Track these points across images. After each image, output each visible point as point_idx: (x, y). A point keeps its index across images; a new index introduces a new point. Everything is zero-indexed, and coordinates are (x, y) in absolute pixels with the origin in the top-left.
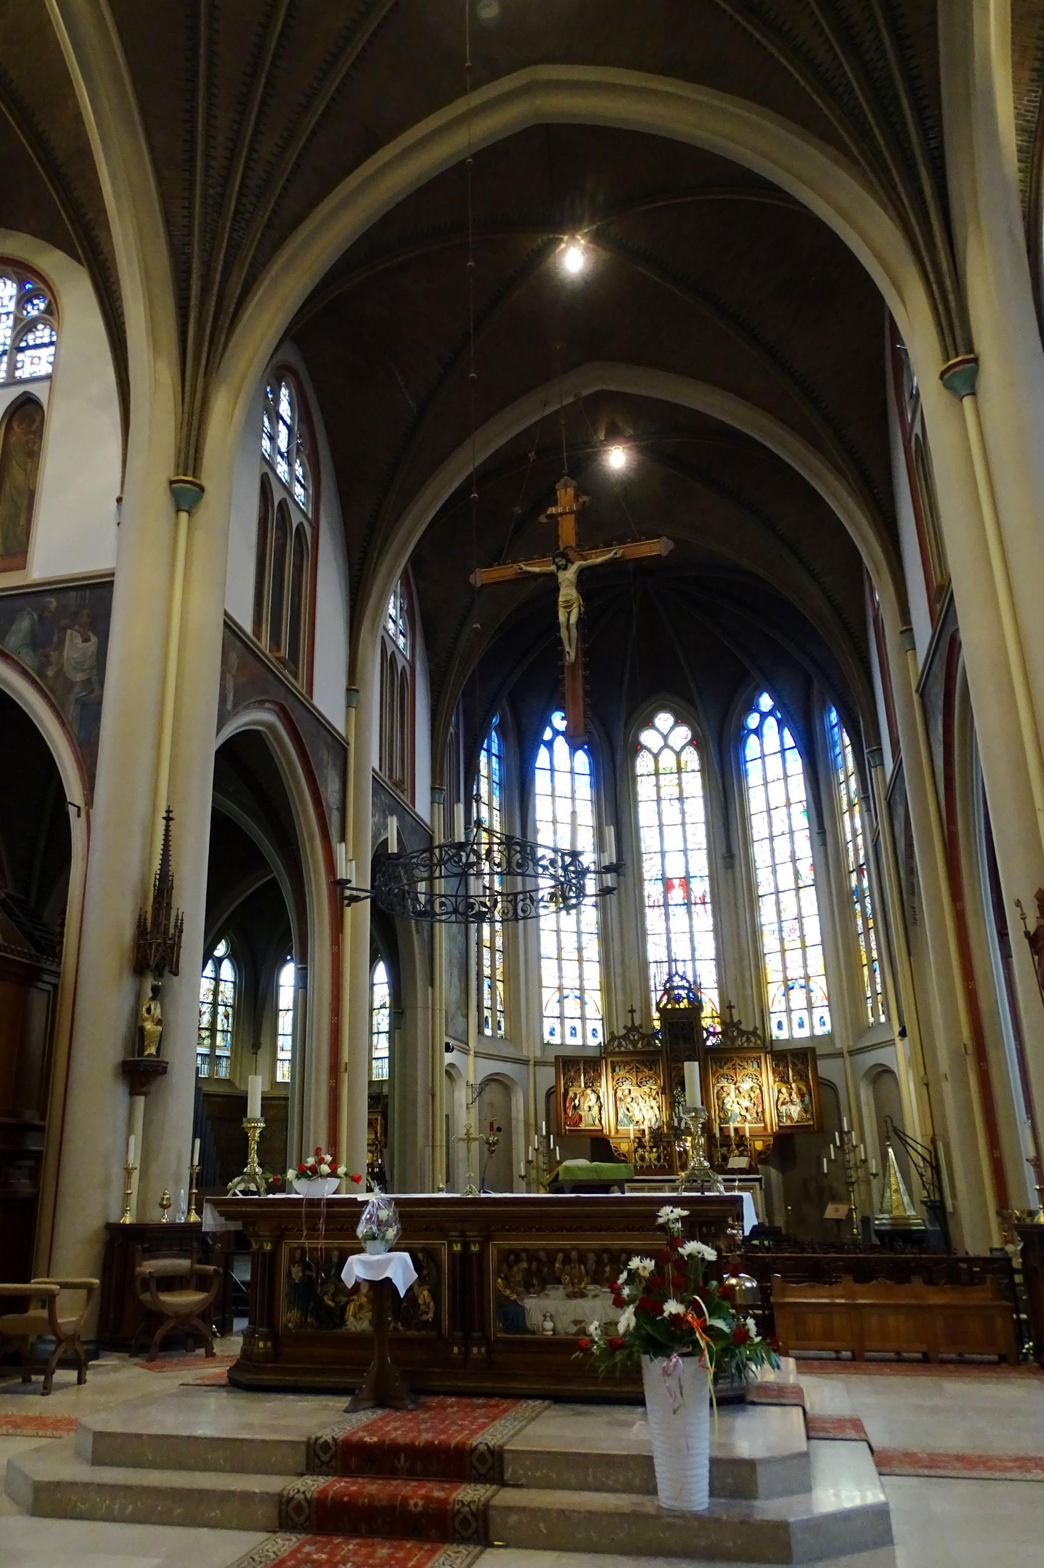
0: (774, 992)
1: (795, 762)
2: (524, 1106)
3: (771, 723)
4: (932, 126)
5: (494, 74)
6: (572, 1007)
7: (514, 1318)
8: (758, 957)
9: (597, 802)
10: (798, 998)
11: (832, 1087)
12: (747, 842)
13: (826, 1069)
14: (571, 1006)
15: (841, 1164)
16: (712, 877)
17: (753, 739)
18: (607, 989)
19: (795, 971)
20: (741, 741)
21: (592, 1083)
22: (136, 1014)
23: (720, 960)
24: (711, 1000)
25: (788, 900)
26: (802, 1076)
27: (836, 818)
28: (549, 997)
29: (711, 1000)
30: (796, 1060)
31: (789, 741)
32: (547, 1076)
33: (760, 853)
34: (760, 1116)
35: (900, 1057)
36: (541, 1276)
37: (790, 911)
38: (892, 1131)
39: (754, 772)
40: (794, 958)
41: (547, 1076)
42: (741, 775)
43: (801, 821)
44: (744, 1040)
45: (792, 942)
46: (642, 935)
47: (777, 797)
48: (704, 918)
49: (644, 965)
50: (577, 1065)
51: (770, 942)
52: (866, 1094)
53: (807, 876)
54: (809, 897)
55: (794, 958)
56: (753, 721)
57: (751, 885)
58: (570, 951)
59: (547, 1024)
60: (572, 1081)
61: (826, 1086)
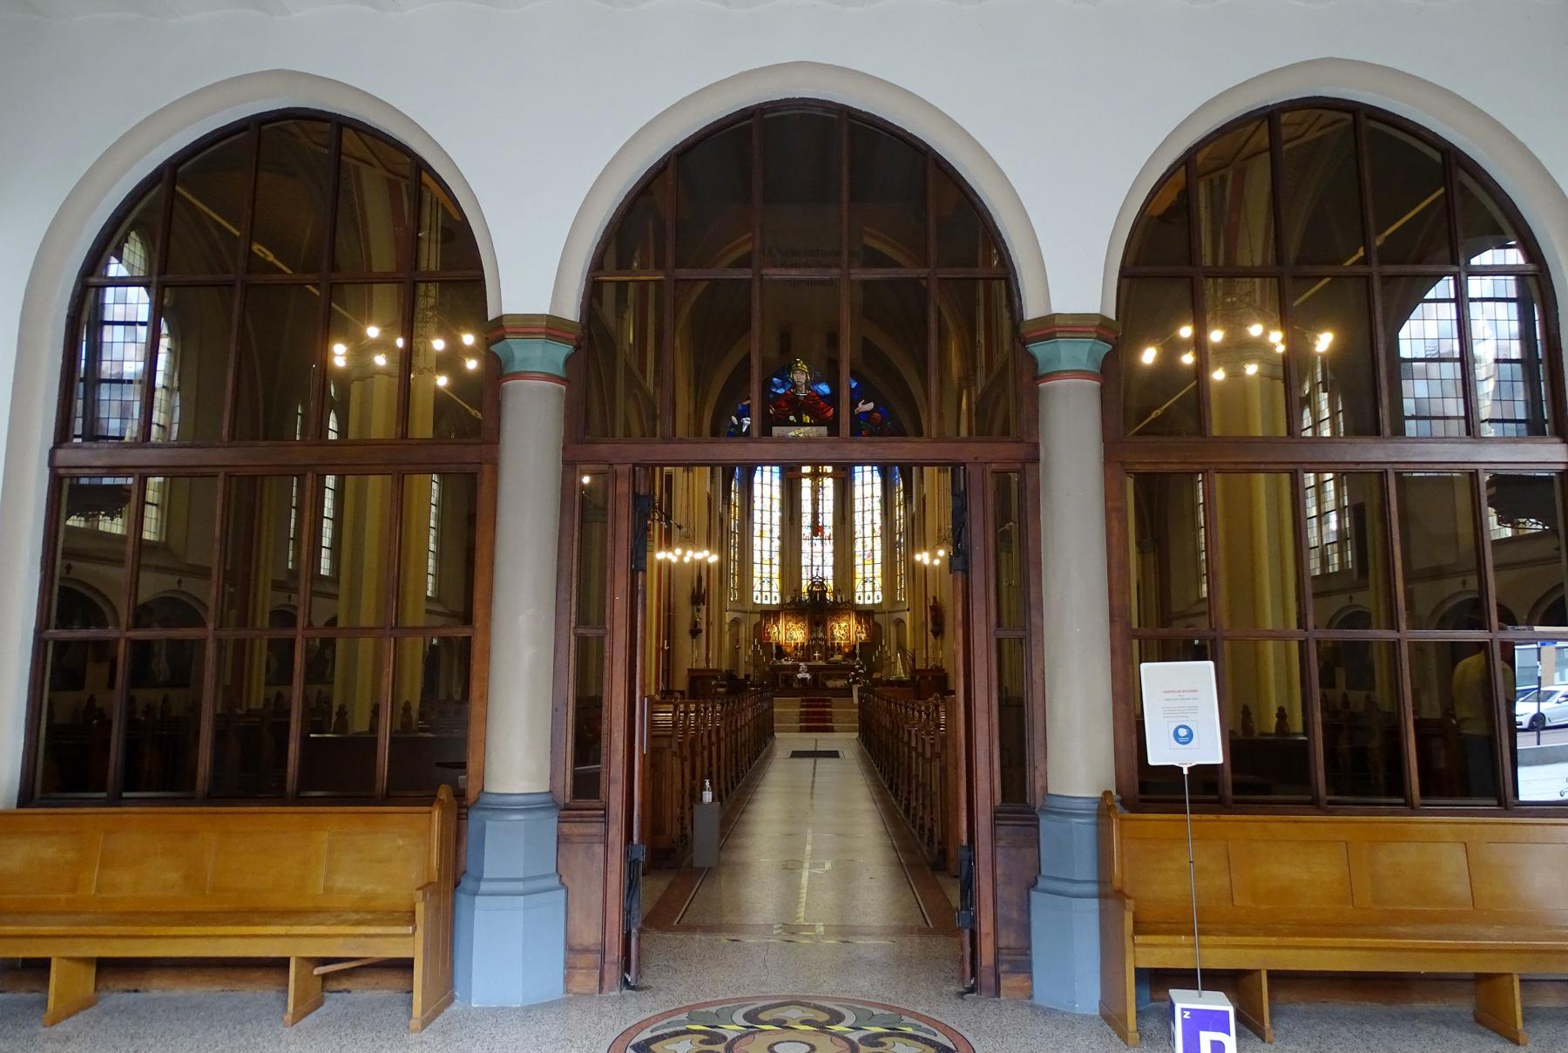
0: (858, 582)
2: (744, 632)
6: (766, 587)
8: (853, 566)
9: (782, 487)
10: (868, 586)
12: (852, 512)
13: (877, 618)
14: (766, 589)
15: (880, 659)
16: (835, 527)
18: (782, 577)
19: (869, 575)
23: (835, 567)
24: (830, 584)
25: (868, 541)
26: (867, 622)
27: (893, 513)
28: (756, 582)
29: (830, 584)
30: (865, 614)
32: (757, 618)
33: (858, 518)
35: (907, 617)
36: (829, 678)
37: (868, 548)
38: (901, 648)
40: (869, 568)
41: (757, 618)
42: (852, 486)
44: (844, 605)
46: (800, 552)
47: (868, 493)
48: (829, 546)
50: (770, 614)
51: (858, 560)
52: (893, 630)
53: (878, 531)
54: (878, 541)
55: (869, 568)
57: (853, 533)
61: (877, 625)
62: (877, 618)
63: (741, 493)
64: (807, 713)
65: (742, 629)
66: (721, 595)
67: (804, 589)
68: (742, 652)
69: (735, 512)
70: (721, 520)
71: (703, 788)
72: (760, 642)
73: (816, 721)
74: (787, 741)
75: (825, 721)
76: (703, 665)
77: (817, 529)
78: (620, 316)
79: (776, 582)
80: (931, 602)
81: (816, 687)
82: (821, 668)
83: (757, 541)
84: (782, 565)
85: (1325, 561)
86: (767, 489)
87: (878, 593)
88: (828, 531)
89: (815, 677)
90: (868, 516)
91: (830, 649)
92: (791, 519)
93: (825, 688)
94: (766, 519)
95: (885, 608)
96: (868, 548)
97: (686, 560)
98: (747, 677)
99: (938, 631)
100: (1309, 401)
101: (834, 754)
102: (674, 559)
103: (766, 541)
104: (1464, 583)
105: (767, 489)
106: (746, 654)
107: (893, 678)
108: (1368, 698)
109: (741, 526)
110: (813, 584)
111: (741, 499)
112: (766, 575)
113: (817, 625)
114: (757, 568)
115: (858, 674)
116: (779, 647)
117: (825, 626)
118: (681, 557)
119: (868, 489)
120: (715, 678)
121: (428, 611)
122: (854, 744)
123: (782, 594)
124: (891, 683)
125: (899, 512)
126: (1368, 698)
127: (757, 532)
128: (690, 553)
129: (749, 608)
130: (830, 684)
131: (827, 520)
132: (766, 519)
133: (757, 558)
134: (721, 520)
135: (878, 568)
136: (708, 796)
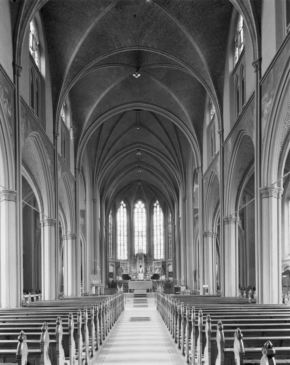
3: (158, 206)
25: (159, 236)
31: (161, 210)
47: (158, 219)
56: (155, 205)
101: (147, 319)
103: (122, 237)
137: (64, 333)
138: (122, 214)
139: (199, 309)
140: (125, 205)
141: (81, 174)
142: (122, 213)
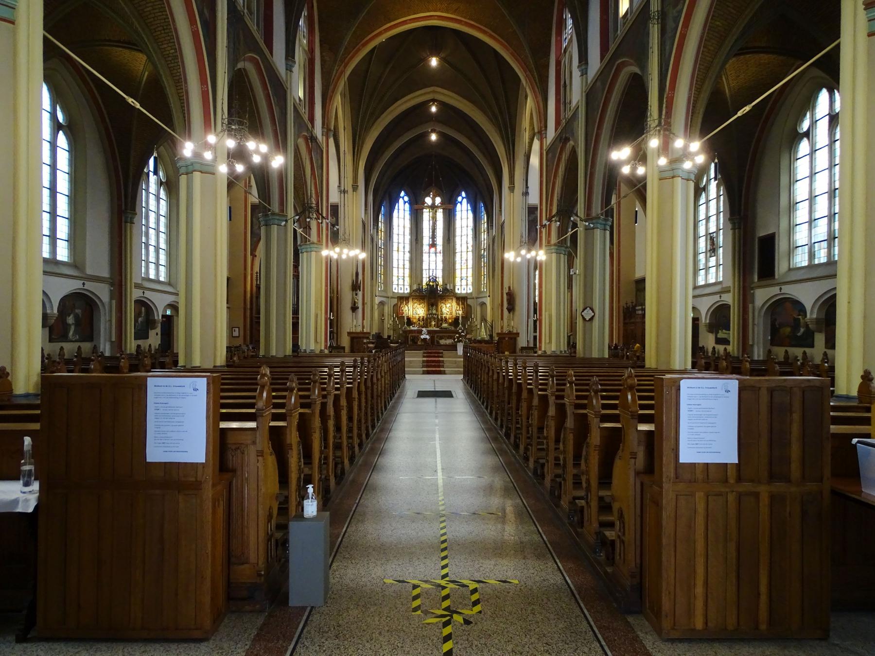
0: (458, 280)
1: (471, 215)
2: (387, 309)
3: (465, 200)
4: (514, 135)
5: (426, 86)
6: (401, 282)
7: (438, 342)
8: (454, 270)
9: (411, 220)
11: (470, 306)
12: (454, 236)
13: (469, 302)
14: (401, 283)
15: (470, 326)
17: (459, 205)
18: (411, 276)
19: (464, 275)
20: (456, 205)
21: (407, 304)
22: (353, 298)
23: (444, 270)
24: (440, 281)
25: (464, 254)
26: (463, 304)
29: (440, 281)
30: (462, 299)
31: (469, 208)
32: (395, 301)
33: (458, 239)
34: (451, 313)
35: (488, 301)
36: (441, 338)
37: (464, 258)
38: (484, 319)
39: (458, 214)
40: (464, 271)
41: (395, 301)
42: (455, 215)
43: (470, 233)
44: (448, 293)
45: (464, 266)
47: (464, 225)
48: (440, 257)
49: (422, 270)
50: (403, 299)
51: (458, 266)
53: (470, 249)
54: (470, 255)
55: (464, 271)
56: (460, 199)
58: (401, 266)
59: (394, 286)
60: (402, 303)
61: (469, 306)
62: (469, 302)
63: (385, 223)
64: (427, 361)
65: (386, 308)
66: (372, 286)
67: (424, 284)
68: (386, 321)
69: (382, 235)
70: (372, 239)
71: (303, 496)
72: (397, 316)
73: (433, 367)
74: (416, 381)
75: (439, 366)
76: (359, 329)
77: (433, 245)
78: (289, 69)
79: (407, 280)
80: (506, 291)
81: (433, 346)
82: (435, 332)
83: (395, 254)
84: (411, 269)
85: (812, 255)
86: (401, 221)
87: (470, 286)
88: (440, 248)
89: (432, 338)
90: (464, 238)
91: (440, 321)
92: (417, 239)
93: (439, 345)
94: (401, 240)
95: (474, 295)
96: (464, 258)
97: (344, 257)
98: (389, 337)
99: (511, 309)
100: (705, 189)
101: (448, 394)
102: (335, 256)
103: (401, 254)
104: (781, 289)
105: (401, 221)
106: (388, 323)
107: (479, 338)
108: (725, 349)
109: (385, 244)
110: (430, 281)
111: (386, 227)
112: (401, 274)
113: (432, 305)
114: (395, 271)
115: (460, 336)
116: (409, 319)
117: (437, 306)
118: (340, 254)
119: (464, 221)
120: (368, 338)
121: (45, 273)
122: (461, 384)
123: (411, 286)
124: (480, 342)
125: (484, 236)
126: (725, 349)
127: (395, 248)
128: (345, 251)
129: (390, 295)
130: (442, 342)
131: (439, 240)
132: (401, 240)
133: (395, 264)
134: (372, 239)
135: (470, 272)
136: (311, 508)
137: (302, 411)
138: (402, 212)
139: (593, 376)
140: (406, 199)
141: (702, 171)
142: (401, 211)
